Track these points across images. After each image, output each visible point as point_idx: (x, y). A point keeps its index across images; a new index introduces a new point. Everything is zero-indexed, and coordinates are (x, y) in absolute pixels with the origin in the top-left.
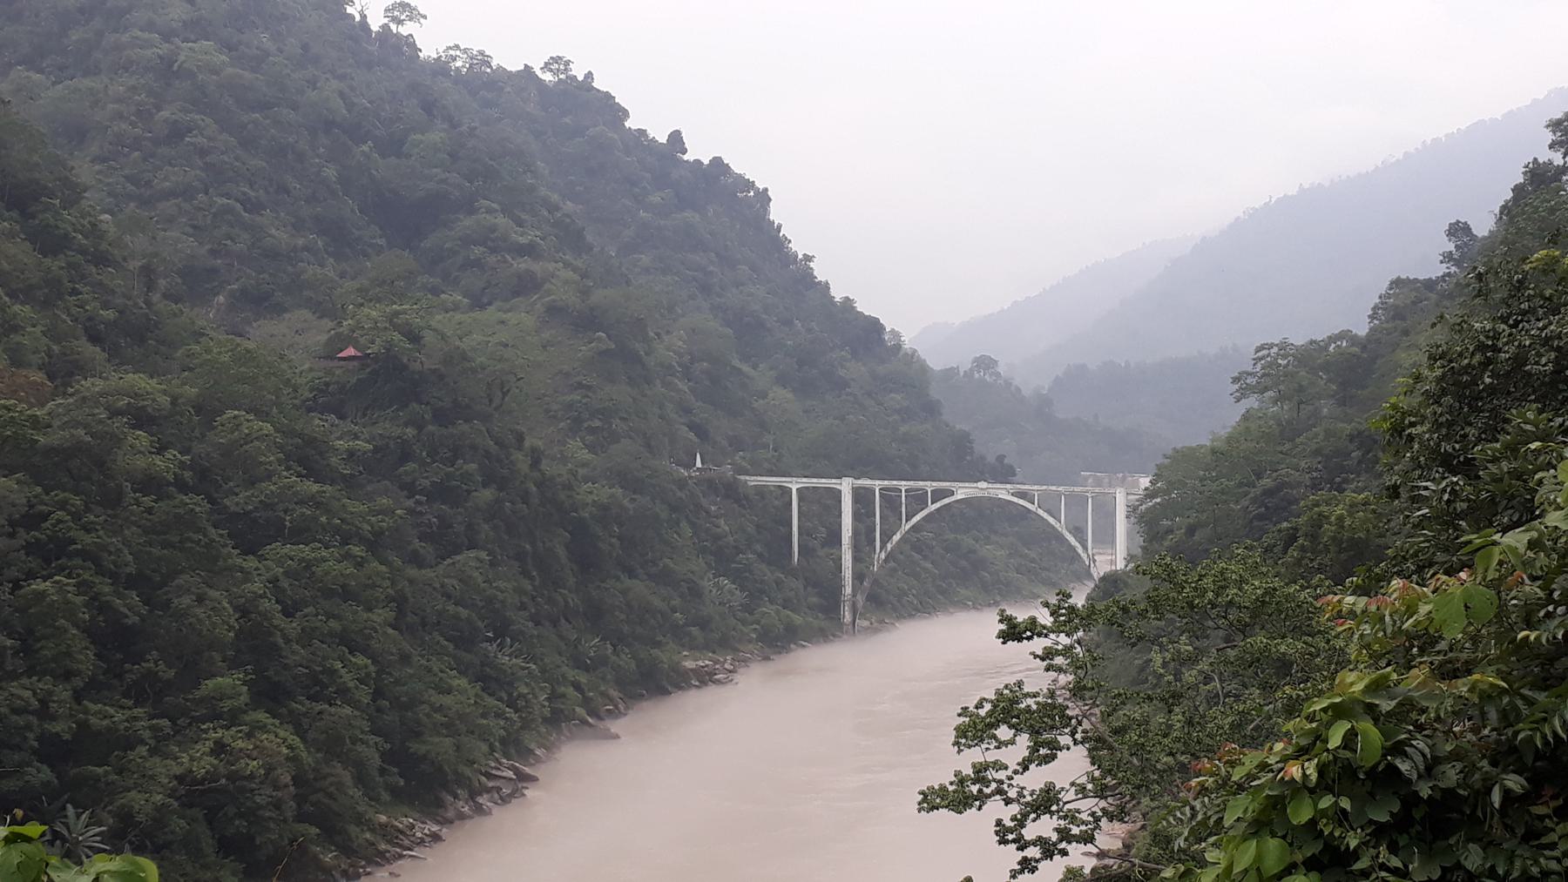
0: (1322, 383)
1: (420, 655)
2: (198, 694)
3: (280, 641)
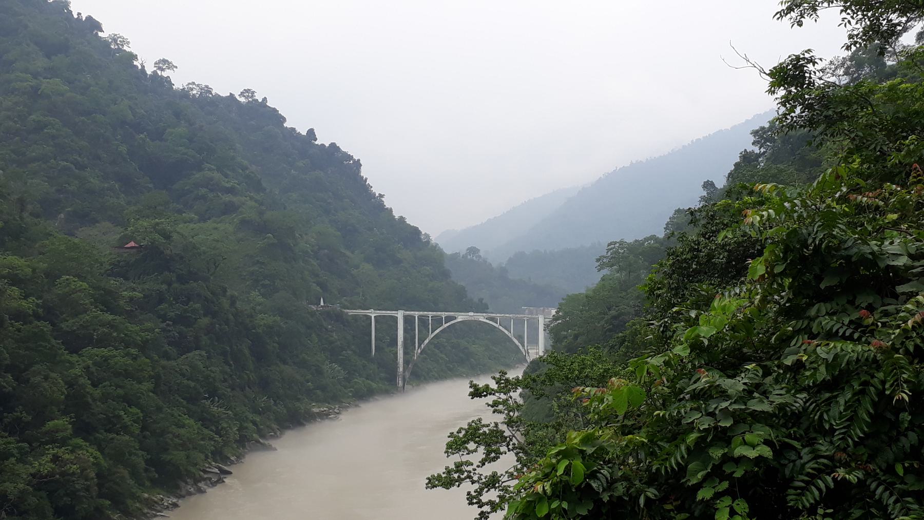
0: (640, 262)
1: (168, 408)
3: (90, 400)
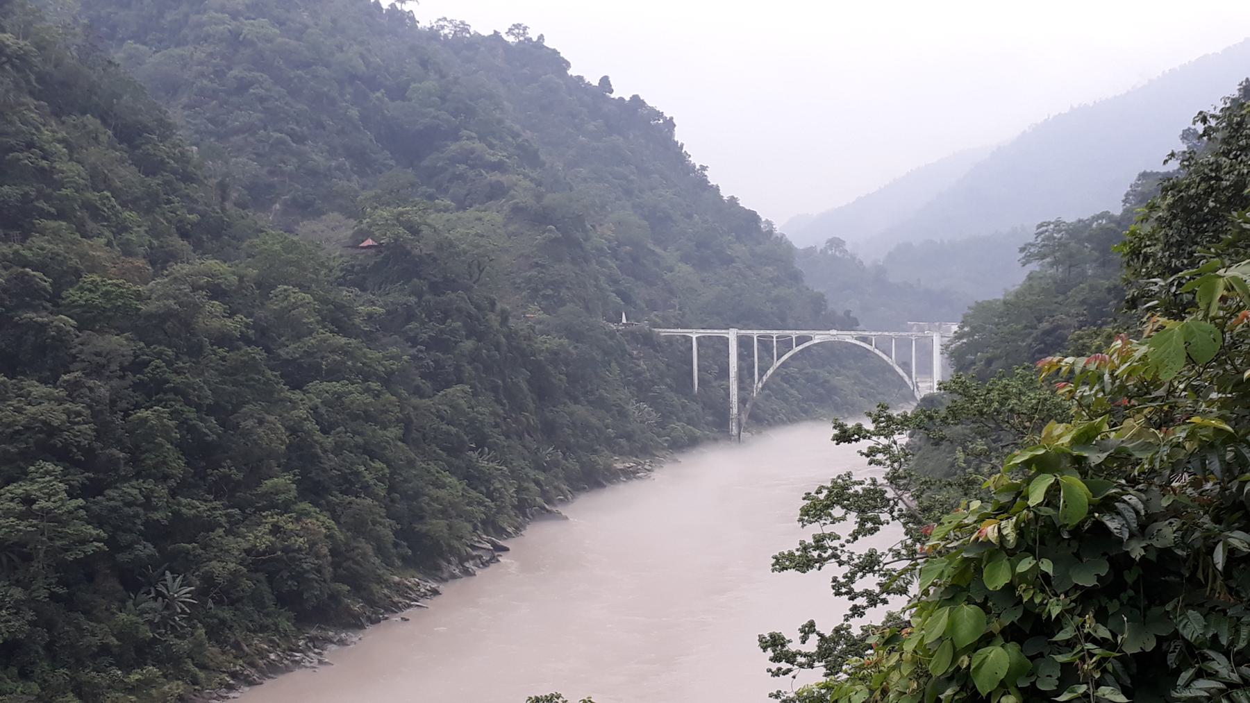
2: (259, 490)
